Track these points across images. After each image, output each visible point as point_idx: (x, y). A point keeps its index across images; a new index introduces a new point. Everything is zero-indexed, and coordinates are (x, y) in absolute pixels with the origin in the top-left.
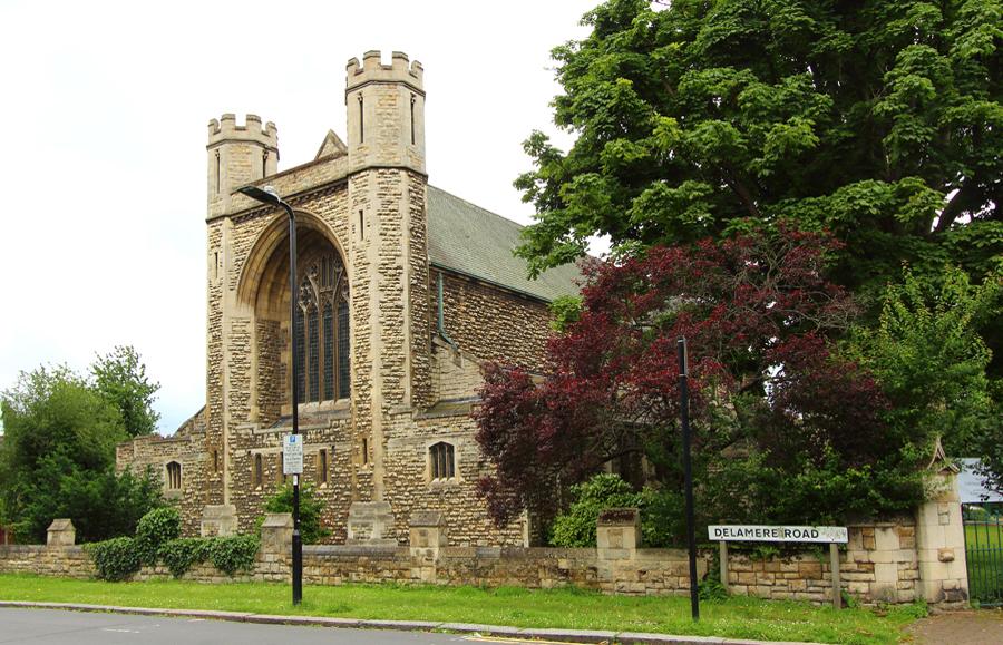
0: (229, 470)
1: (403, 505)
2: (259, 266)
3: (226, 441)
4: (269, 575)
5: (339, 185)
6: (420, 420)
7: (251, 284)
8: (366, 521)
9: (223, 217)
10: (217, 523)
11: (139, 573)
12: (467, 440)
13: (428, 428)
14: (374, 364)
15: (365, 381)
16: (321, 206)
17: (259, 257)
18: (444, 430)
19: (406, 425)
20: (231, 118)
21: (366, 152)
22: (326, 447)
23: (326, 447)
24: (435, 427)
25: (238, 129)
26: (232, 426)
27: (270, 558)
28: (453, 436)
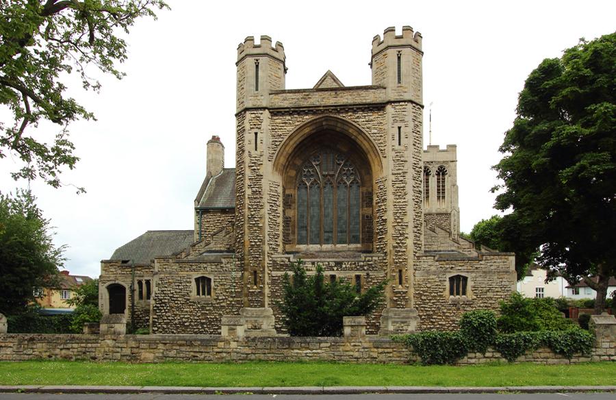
0: (268, 284)
1: (428, 311)
2: (289, 149)
3: (266, 265)
4: (606, 357)
5: (379, 107)
6: (441, 261)
7: (282, 160)
8: (404, 320)
9: (264, 108)
10: (260, 320)
11: (466, 357)
12: (478, 275)
13: (448, 266)
14: (409, 224)
15: (402, 235)
16: (358, 117)
17: (291, 143)
18: (460, 268)
19: (430, 263)
20: (392, 30)
21: (406, 90)
22: (363, 274)
23: (363, 274)
24: (453, 266)
25: (397, 38)
26: (270, 255)
27: (607, 345)
28: (468, 272)
